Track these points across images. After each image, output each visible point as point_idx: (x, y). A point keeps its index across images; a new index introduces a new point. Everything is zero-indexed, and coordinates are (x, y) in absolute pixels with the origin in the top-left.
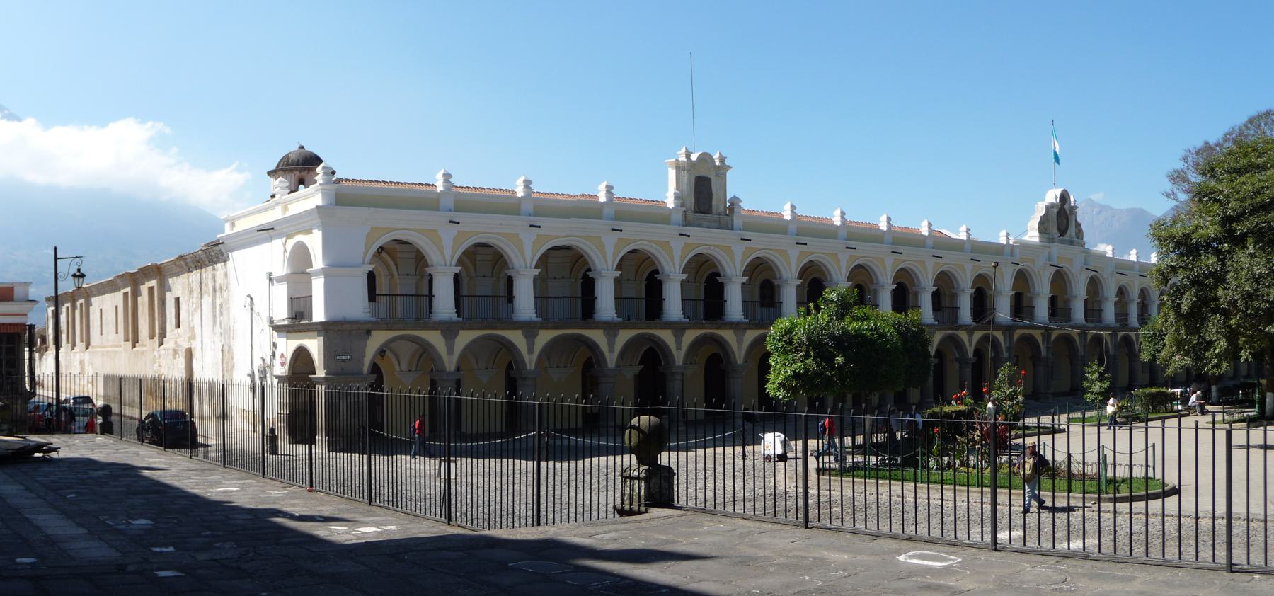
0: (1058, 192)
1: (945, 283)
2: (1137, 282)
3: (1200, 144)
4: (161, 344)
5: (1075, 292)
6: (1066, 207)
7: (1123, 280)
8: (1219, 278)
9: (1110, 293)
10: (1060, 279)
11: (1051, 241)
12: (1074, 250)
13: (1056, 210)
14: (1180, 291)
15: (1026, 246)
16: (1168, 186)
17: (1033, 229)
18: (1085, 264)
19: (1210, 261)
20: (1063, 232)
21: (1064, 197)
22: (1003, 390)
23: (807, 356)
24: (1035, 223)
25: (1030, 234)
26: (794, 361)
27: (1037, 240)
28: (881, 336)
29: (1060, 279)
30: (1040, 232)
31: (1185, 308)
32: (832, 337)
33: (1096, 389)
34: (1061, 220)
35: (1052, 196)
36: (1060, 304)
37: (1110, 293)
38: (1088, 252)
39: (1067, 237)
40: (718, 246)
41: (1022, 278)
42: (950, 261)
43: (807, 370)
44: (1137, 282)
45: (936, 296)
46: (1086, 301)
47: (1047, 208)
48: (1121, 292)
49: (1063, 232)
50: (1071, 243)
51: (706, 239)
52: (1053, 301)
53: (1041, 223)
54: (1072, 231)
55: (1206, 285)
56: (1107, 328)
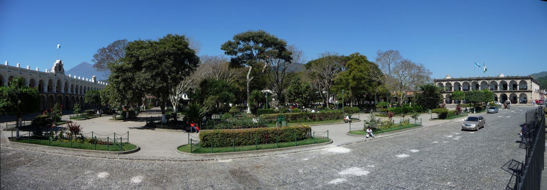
1: (41, 82)
3: (102, 48)
8: (133, 79)
10: (59, 82)
11: (57, 72)
14: (118, 83)
15: (52, 73)
16: (93, 58)
19: (129, 74)
20: (60, 70)
21: (60, 62)
22: (55, 109)
23: (8, 100)
24: (53, 68)
26: (3, 102)
28: (33, 94)
29: (59, 82)
31: (121, 88)
32: (17, 94)
33: (77, 110)
34: (59, 67)
35: (58, 61)
37: (70, 86)
38: (65, 76)
41: (50, 81)
42: (34, 76)
43: (8, 105)
45: (39, 85)
48: (72, 86)
49: (60, 70)
54: (62, 70)
55: (128, 82)
56: (69, 94)
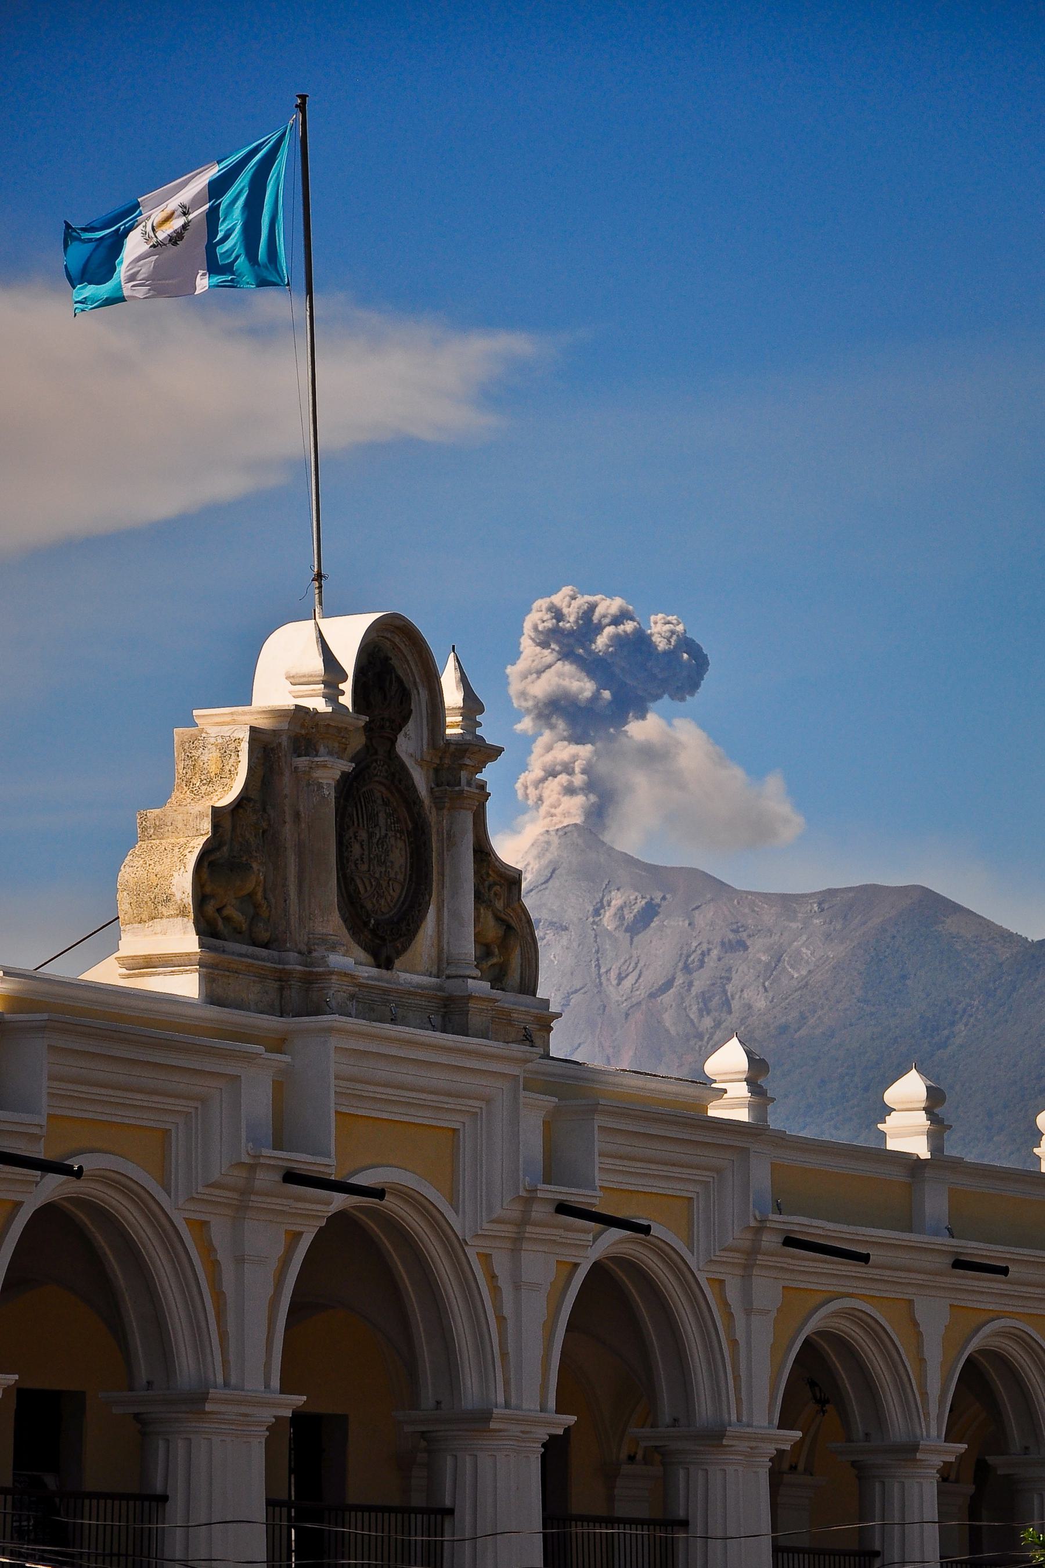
0: (348, 635)
2: (933, 1316)
4: (66, 266)
5: (898, 1428)
6: (408, 745)
7: (836, 1299)
9: (744, 1390)
10: (363, 1279)
12: (479, 1061)
13: (330, 770)
17: (153, 907)
18: (552, 1169)
24: (170, 860)
25: (135, 942)
27: (186, 985)
29: (363, 1279)
30: (209, 925)
35: (295, 667)
36: (364, 1477)
39: (412, 974)
40: (613, 1244)
44: (933, 1316)
46: (555, 1453)
47: (262, 745)
48: (822, 1380)
50: (449, 1013)
51: (368, 1073)
52: (308, 1450)
53: (210, 865)
54: (451, 925)
